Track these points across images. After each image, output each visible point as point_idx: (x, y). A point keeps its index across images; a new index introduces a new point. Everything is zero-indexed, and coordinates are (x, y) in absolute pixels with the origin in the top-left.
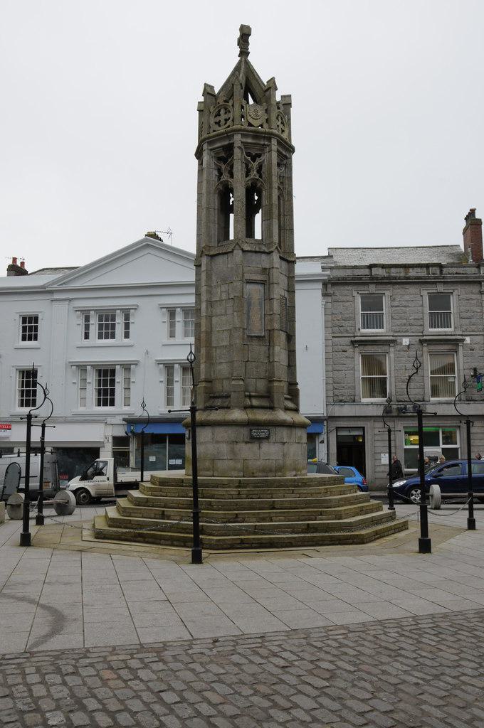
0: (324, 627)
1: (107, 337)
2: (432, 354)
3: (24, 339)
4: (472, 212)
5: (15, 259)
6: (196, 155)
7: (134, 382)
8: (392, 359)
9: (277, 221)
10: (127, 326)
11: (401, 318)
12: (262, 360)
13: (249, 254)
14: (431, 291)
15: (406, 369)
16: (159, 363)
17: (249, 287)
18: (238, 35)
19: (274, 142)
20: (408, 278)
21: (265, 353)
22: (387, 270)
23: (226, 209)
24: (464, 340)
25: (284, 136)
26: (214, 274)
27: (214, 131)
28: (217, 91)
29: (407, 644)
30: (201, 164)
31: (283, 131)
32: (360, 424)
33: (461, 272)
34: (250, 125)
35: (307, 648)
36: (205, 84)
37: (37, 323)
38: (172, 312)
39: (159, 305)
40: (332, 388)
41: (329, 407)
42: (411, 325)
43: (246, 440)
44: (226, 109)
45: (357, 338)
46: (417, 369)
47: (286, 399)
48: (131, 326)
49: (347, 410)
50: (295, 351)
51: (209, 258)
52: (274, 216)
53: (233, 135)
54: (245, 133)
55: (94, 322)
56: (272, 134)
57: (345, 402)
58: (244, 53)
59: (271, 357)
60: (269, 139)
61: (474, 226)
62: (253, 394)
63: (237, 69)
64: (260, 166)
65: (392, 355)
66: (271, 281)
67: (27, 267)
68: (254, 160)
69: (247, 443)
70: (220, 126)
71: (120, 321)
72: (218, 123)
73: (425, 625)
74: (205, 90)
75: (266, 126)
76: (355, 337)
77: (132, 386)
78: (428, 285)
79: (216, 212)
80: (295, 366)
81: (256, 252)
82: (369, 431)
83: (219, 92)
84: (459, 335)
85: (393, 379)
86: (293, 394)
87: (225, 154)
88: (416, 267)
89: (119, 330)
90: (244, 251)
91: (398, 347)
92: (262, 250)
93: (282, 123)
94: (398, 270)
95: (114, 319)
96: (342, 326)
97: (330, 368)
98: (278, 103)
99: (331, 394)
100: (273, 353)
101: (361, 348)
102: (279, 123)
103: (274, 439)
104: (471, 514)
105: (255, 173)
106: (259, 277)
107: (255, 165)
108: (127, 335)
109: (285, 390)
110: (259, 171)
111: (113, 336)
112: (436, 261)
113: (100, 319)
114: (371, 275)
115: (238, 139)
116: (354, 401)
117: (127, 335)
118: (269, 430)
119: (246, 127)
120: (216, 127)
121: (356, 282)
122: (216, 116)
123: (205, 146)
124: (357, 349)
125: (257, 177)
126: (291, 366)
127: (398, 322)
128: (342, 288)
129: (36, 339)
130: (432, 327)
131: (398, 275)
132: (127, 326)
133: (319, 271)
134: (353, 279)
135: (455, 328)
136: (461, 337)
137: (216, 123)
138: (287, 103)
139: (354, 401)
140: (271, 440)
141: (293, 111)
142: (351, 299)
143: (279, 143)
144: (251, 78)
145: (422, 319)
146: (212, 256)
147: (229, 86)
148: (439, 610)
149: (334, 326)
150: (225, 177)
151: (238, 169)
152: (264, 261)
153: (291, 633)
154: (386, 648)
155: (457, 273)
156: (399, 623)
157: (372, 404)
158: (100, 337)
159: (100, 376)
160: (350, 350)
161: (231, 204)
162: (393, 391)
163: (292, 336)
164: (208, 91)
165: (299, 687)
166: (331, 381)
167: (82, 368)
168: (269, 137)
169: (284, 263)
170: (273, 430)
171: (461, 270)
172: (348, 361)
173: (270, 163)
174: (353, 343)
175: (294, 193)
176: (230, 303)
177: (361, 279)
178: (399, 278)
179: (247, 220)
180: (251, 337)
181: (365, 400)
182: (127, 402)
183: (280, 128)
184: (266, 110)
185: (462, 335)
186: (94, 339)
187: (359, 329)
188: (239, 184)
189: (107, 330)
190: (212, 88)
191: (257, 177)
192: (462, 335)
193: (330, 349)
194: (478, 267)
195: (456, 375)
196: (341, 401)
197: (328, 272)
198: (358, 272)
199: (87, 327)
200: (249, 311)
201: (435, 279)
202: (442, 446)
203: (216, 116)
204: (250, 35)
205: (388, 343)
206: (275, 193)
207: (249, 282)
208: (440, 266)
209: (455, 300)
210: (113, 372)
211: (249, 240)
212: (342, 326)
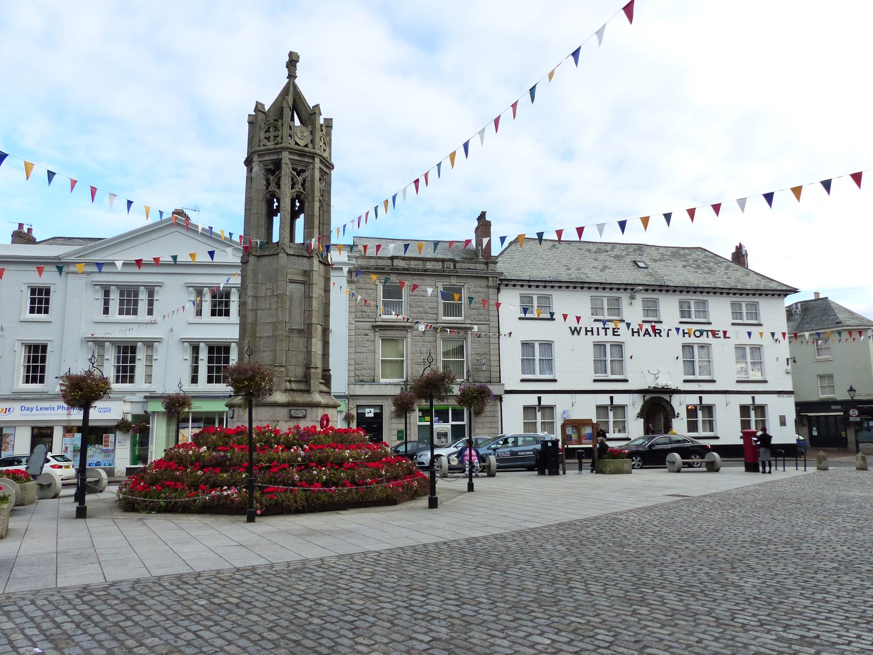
0: (363, 553)
1: (128, 313)
2: (445, 340)
3: (32, 311)
4: (483, 214)
5: (21, 226)
6: (245, 163)
7: (156, 360)
8: (409, 344)
9: (317, 230)
10: (151, 303)
11: (418, 306)
12: (301, 350)
13: (293, 257)
14: (445, 284)
15: (421, 353)
16: (183, 341)
17: (291, 286)
18: (287, 59)
19: (317, 160)
20: (426, 270)
21: (304, 343)
22: (407, 261)
23: (272, 213)
24: (473, 328)
25: (325, 155)
26: (260, 273)
27: (264, 145)
28: (267, 108)
29: (420, 558)
30: (250, 170)
31: (325, 150)
32: (378, 402)
33: (472, 268)
34: (297, 144)
35: (354, 563)
36: (257, 102)
37: (49, 295)
38: (199, 292)
39: (186, 283)
40: (353, 369)
41: (351, 386)
42: (426, 313)
43: (286, 419)
44: (275, 127)
45: (378, 324)
46: (430, 363)
47: (321, 383)
48: (155, 303)
49: (367, 390)
50: (329, 342)
51: (256, 258)
52: (315, 226)
53: (282, 151)
54: (292, 151)
55: (115, 296)
56: (316, 154)
57: (365, 382)
58: (292, 76)
59: (309, 347)
60: (313, 158)
61: (484, 227)
62: (292, 379)
63: (285, 91)
64: (304, 181)
65: (409, 340)
66: (311, 281)
67: (34, 234)
68: (299, 174)
69: (286, 422)
70: (269, 141)
71: (143, 296)
72: (268, 139)
73: (431, 548)
74: (256, 106)
75: (310, 146)
76: (376, 322)
77: (154, 363)
78: (444, 278)
79: (263, 218)
80: (329, 355)
81: (298, 256)
82: (387, 409)
83: (269, 110)
84: (468, 324)
85: (409, 362)
86: (326, 379)
87: (273, 167)
88: (432, 261)
89: (143, 306)
90: (288, 254)
91: (415, 333)
92: (306, 252)
93: (324, 143)
94: (417, 262)
95: (136, 294)
96: (365, 312)
97: (353, 350)
98: (321, 126)
99: (352, 374)
100: (311, 344)
101: (382, 332)
102: (322, 143)
103: (310, 418)
104: (471, 480)
105: (300, 186)
106: (301, 278)
107: (300, 179)
108: (150, 312)
109: (320, 376)
110: (303, 185)
111: (135, 312)
112: (450, 257)
113: (122, 294)
114: (393, 266)
115: (286, 156)
116: (373, 381)
117: (150, 312)
118: (306, 410)
119: (293, 145)
120: (265, 142)
121: (378, 270)
122: (266, 132)
123: (255, 158)
124: (378, 334)
125: (302, 190)
126: (326, 355)
127: (415, 310)
128: (366, 277)
129: (46, 311)
130: (445, 316)
131: (417, 267)
132: (151, 303)
133: (346, 260)
134: (376, 269)
135: (465, 317)
136: (469, 326)
137: (266, 138)
138: (329, 123)
139: (374, 381)
140: (307, 419)
141: (334, 132)
142: (374, 287)
143: (321, 161)
144: (298, 100)
145: (437, 308)
146: (258, 257)
147: (279, 105)
148: (441, 540)
149: (358, 312)
150: (273, 187)
151: (286, 182)
152: (304, 264)
153: (340, 557)
154: (405, 560)
155: (468, 269)
156: (414, 549)
157: (390, 384)
158: (121, 312)
159: (119, 353)
160: (371, 334)
161: (275, 208)
162: (410, 374)
163: (327, 329)
164: (259, 108)
165: (352, 580)
166: (353, 362)
167: (99, 343)
168: (312, 156)
169: (322, 266)
170: (309, 410)
171: (472, 266)
172: (368, 344)
173: (313, 180)
174: (374, 327)
175: (332, 204)
176: (275, 299)
177: (383, 269)
178: (418, 270)
179: (290, 227)
180: (293, 329)
181: (383, 381)
182: (149, 378)
183: (322, 148)
184: (311, 132)
185: (471, 324)
186: (114, 313)
187: (380, 315)
188: (286, 193)
189: (129, 305)
190: (263, 105)
191: (302, 190)
192: (471, 324)
193: (353, 333)
194: (487, 264)
195: (465, 359)
196: (362, 381)
197: (353, 262)
198: (381, 263)
199: (106, 302)
200: (290, 308)
201: (449, 272)
202: (451, 423)
203: (266, 132)
204: (298, 61)
205: (404, 328)
206: (317, 205)
207: (292, 281)
208: (454, 261)
209: (465, 292)
210: (134, 350)
211: (292, 245)
212: (365, 312)
